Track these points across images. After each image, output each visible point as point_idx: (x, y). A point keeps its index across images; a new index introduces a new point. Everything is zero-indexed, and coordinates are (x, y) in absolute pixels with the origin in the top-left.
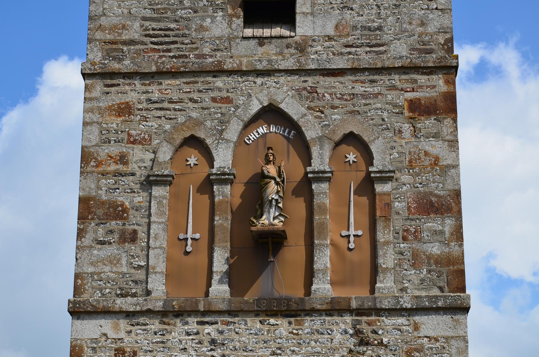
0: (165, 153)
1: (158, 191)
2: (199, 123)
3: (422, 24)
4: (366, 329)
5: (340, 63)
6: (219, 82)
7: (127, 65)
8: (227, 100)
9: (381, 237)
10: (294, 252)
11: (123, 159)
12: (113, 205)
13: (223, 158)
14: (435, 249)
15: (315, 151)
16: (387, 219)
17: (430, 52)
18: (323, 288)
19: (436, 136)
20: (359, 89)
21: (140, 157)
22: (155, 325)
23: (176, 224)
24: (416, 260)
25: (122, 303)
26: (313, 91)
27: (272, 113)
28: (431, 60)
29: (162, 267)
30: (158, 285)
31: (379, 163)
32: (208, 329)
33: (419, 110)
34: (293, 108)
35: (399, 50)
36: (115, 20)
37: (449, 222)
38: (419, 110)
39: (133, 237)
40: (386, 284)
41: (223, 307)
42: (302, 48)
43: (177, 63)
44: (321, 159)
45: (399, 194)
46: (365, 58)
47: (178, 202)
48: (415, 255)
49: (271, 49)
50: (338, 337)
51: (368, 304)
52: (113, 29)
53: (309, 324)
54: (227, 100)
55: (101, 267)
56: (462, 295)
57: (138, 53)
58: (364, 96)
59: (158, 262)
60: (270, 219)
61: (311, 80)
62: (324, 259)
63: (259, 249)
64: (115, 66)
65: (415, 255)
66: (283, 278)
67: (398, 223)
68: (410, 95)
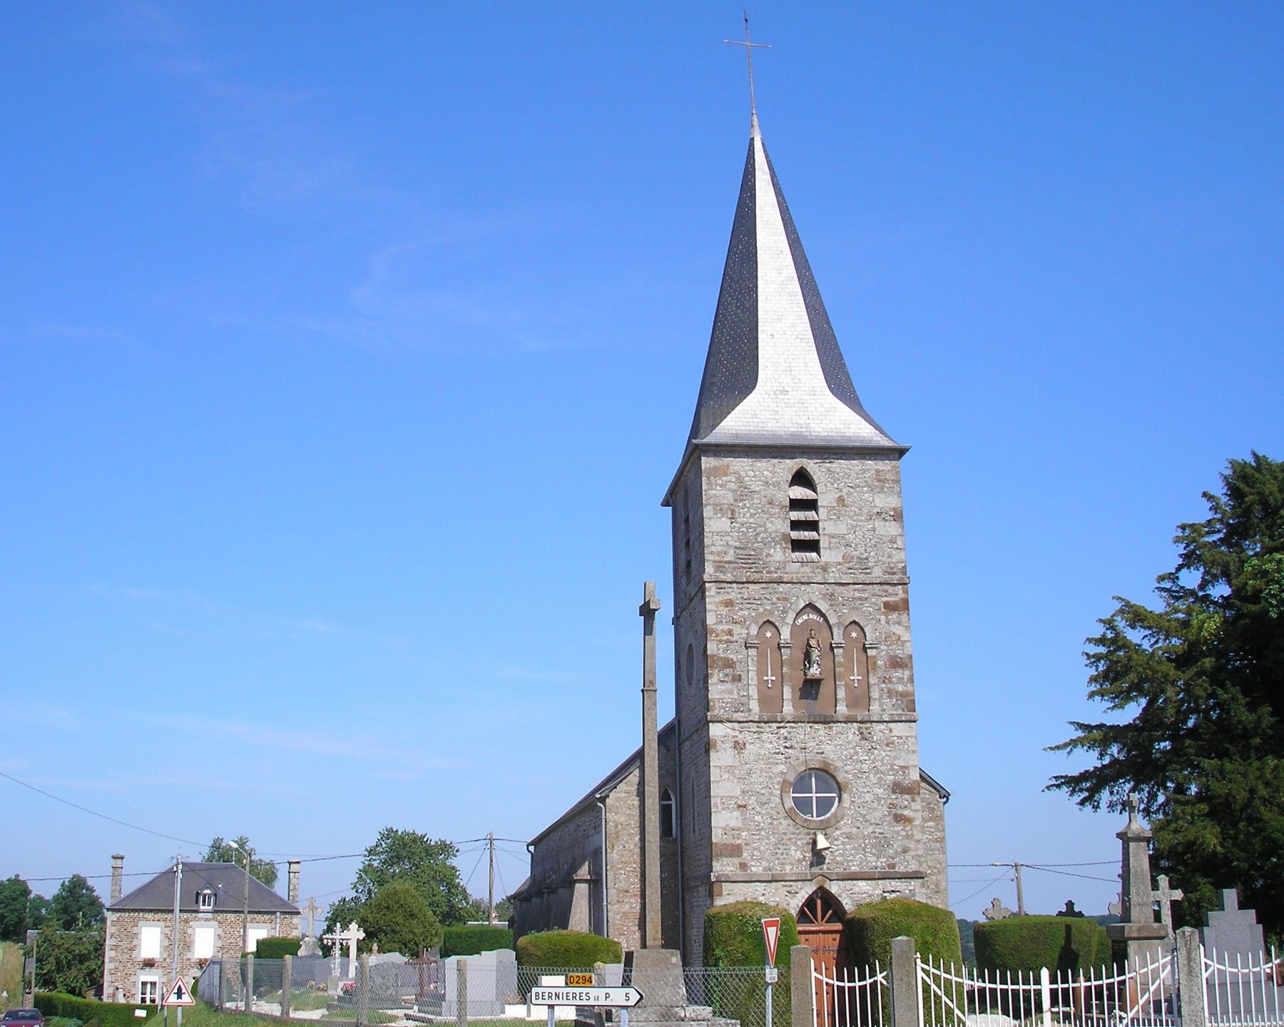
0: (754, 630)
1: (753, 652)
2: (771, 612)
3: (890, 557)
4: (865, 732)
5: (846, 579)
6: (781, 588)
7: (729, 577)
8: (785, 599)
9: (872, 681)
10: (825, 689)
11: (730, 633)
12: (727, 660)
13: (786, 634)
14: (900, 688)
15: (835, 630)
16: (874, 669)
17: (894, 573)
18: (842, 709)
19: (899, 623)
20: (857, 594)
21: (739, 632)
22: (754, 727)
23: (761, 672)
24: (891, 693)
25: (736, 716)
26: (832, 595)
27: (811, 607)
28: (895, 579)
29: (756, 696)
30: (754, 706)
31: (870, 638)
32: (782, 731)
33: (890, 607)
34: (823, 606)
35: (877, 574)
36: (720, 549)
37: (907, 673)
38: (890, 607)
39: (739, 679)
40: (875, 707)
41: (789, 718)
42: (825, 569)
43: (757, 576)
44: (838, 637)
45: (880, 655)
46: (862, 578)
47: (762, 656)
48: (890, 691)
49: (807, 569)
50: (851, 736)
51: (866, 719)
52: (719, 553)
53: (837, 727)
54: (785, 599)
55: (723, 696)
56: (564, 932)
57: (734, 569)
58: (860, 599)
59: (753, 691)
60: (814, 671)
61: (831, 588)
62: (841, 694)
63: (810, 688)
64: (722, 577)
65: (890, 691)
66: (820, 705)
67: (881, 673)
68: (885, 599)
